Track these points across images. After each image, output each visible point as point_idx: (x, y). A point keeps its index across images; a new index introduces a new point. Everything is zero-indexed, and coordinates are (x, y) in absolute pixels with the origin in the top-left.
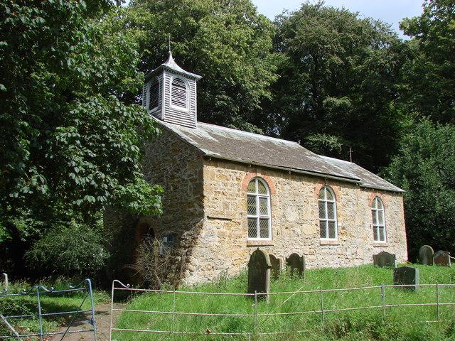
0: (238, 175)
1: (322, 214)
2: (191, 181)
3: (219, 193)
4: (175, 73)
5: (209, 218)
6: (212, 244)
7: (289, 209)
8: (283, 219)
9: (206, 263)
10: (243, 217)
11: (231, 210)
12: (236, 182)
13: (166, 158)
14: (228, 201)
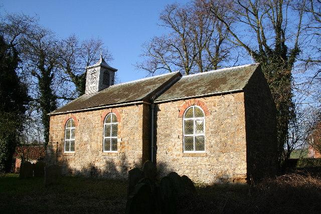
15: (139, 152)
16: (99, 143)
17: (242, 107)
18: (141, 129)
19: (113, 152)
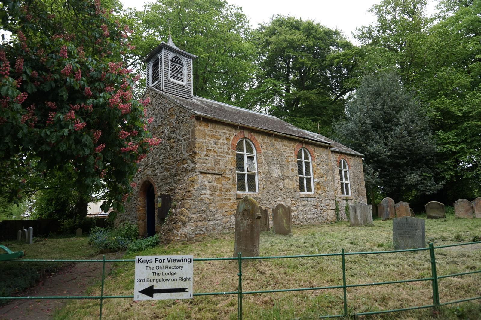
0: (228, 136)
1: (300, 172)
2: (184, 139)
3: (210, 150)
4: (173, 52)
5: (201, 173)
6: (204, 196)
7: (273, 167)
8: (268, 175)
9: (198, 215)
10: (232, 173)
11: (222, 166)
12: (225, 142)
13: (164, 122)
14: (219, 158)
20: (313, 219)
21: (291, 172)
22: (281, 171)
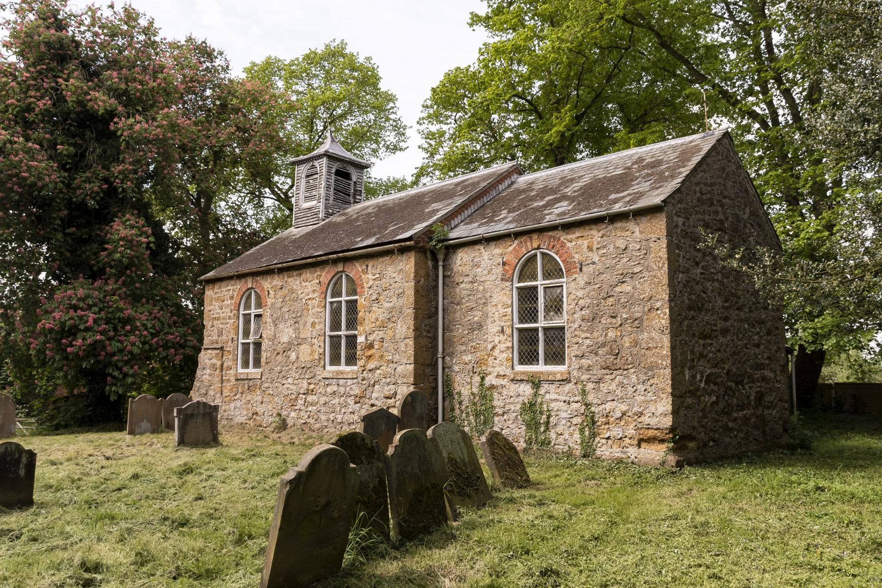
1: (336, 326)
7: (281, 326)
15: (407, 368)
16: (316, 347)
17: (660, 250)
18: (410, 311)
19: (349, 368)
20: (349, 424)
21: (311, 329)
22: (295, 330)
